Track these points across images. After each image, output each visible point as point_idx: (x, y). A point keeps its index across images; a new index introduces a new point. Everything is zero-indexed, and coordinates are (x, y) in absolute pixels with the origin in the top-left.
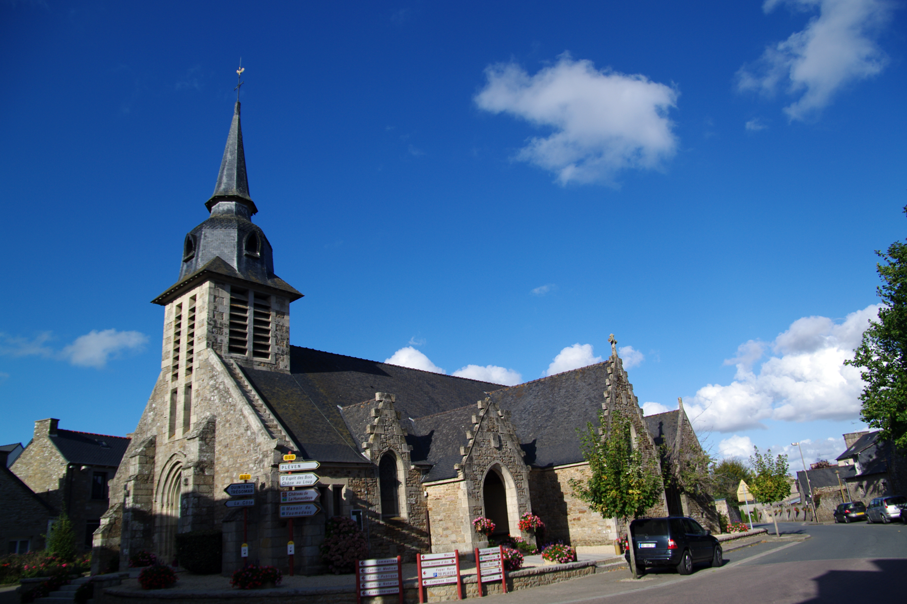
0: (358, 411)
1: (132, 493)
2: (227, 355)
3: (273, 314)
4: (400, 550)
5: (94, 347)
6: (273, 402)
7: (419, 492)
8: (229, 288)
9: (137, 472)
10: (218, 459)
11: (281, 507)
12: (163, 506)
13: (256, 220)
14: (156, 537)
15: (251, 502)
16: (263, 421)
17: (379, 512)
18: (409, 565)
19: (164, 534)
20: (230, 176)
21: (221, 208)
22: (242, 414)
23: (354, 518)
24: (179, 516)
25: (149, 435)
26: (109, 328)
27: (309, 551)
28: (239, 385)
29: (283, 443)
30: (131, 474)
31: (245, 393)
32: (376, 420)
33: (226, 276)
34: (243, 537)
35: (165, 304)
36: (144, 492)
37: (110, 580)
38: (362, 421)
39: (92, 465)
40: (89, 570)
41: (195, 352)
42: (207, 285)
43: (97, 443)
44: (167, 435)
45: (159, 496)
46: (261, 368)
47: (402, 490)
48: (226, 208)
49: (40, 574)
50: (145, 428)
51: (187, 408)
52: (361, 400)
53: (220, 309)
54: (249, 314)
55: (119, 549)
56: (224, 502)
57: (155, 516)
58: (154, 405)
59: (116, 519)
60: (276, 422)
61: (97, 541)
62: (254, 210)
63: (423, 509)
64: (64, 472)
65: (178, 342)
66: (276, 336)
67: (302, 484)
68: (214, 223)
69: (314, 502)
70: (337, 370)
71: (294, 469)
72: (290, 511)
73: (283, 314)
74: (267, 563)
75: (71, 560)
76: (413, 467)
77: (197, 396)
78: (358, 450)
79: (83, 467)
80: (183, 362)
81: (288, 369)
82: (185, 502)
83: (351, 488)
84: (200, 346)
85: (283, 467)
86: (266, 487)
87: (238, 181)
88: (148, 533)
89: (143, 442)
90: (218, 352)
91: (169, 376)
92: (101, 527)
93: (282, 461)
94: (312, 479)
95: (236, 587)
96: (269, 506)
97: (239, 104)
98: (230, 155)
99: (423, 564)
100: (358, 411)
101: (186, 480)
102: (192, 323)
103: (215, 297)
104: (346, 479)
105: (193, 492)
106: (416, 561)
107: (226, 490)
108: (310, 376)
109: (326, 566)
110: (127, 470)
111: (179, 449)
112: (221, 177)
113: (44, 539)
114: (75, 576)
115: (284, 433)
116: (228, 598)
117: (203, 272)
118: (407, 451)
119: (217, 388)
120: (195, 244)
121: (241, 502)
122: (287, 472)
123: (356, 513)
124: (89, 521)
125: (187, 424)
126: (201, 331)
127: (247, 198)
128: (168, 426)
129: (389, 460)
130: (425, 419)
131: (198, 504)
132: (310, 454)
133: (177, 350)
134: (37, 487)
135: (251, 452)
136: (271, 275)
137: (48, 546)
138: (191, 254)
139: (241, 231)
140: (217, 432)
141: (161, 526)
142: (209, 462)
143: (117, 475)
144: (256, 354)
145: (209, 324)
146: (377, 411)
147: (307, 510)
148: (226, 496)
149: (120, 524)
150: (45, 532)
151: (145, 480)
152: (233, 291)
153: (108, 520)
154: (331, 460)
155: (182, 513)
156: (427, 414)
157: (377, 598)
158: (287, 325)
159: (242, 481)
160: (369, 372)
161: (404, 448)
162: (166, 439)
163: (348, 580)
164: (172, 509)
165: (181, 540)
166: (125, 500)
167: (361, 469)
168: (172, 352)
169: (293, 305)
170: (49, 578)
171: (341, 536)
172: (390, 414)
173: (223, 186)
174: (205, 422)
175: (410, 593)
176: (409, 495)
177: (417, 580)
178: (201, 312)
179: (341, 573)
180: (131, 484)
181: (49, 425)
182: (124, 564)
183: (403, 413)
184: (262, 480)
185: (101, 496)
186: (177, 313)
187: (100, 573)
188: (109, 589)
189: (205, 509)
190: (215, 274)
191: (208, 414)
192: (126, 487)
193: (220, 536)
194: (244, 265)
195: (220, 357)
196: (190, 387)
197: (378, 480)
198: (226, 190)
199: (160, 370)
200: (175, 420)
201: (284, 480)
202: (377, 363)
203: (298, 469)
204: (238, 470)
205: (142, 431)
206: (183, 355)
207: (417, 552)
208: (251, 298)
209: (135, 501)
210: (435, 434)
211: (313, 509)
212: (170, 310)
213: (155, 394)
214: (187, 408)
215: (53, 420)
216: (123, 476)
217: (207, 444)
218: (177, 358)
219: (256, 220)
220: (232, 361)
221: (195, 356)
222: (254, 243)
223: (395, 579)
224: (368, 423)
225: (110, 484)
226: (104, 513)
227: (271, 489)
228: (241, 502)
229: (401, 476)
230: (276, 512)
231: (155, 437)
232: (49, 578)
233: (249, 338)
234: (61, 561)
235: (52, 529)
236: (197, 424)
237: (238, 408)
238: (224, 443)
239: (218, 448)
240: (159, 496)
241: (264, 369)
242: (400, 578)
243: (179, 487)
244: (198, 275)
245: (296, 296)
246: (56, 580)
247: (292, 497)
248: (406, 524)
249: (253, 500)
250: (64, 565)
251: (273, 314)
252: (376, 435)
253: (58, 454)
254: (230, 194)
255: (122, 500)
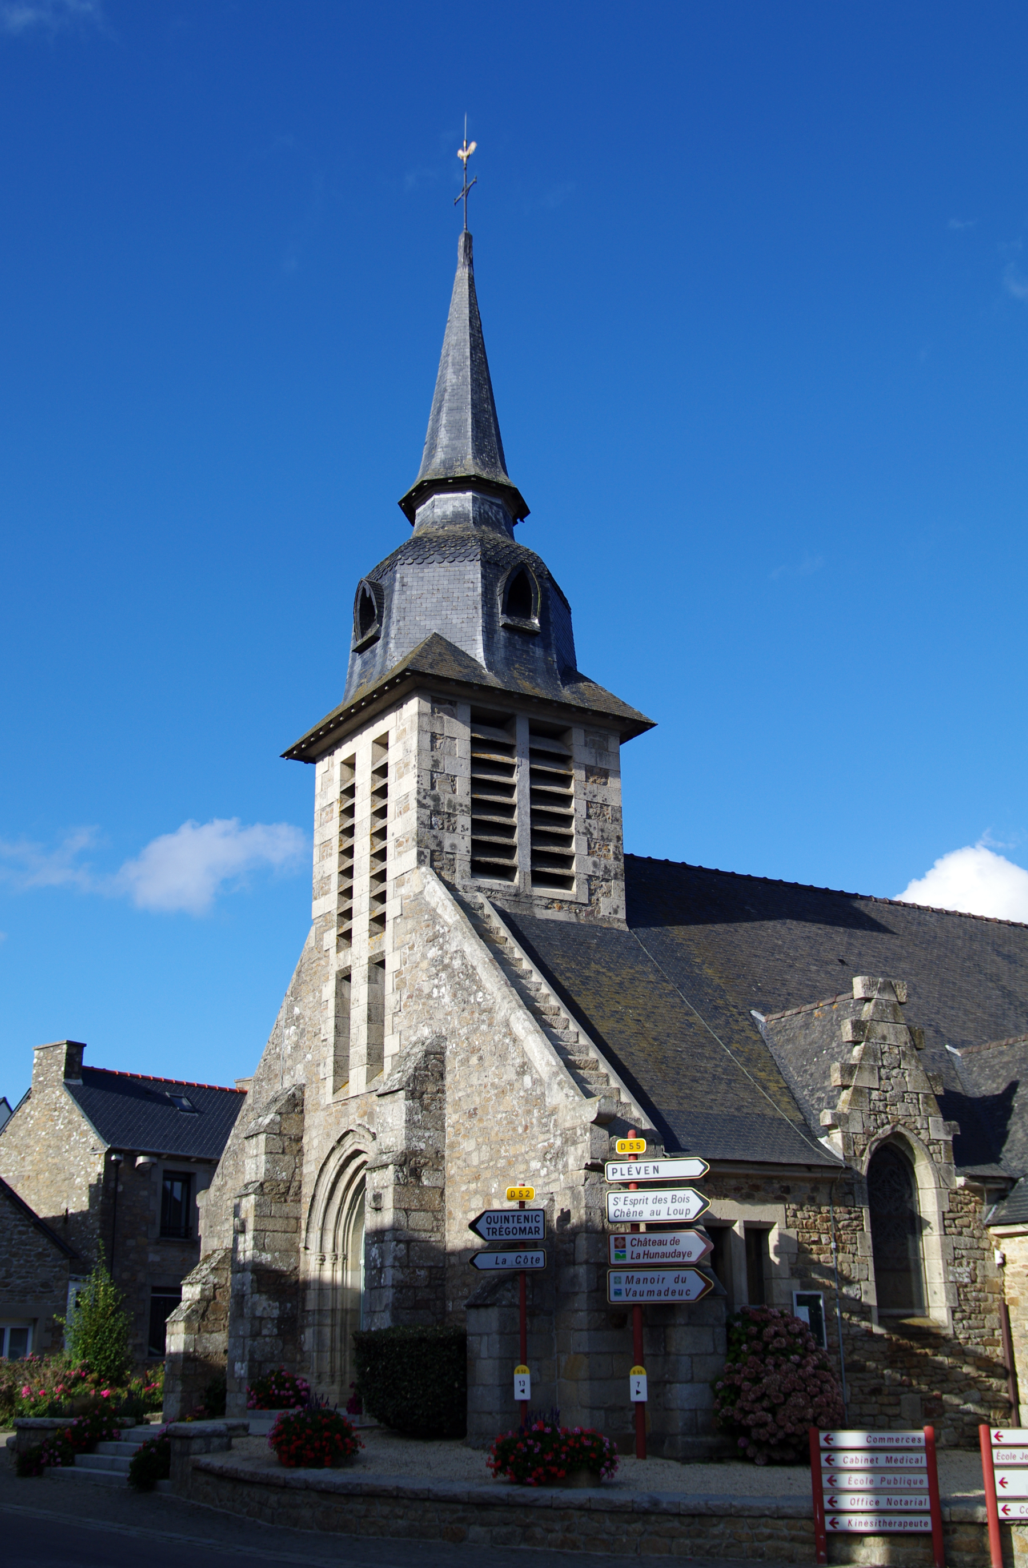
0: (807, 1026)
1: (250, 1225)
2: (468, 882)
3: (578, 775)
4: (931, 1411)
5: (187, 864)
6: (584, 1002)
7: (980, 1252)
8: (466, 712)
9: (261, 1176)
10: (452, 1146)
11: (613, 1275)
12: (323, 1260)
13: (526, 536)
14: (308, 1337)
15: (536, 1259)
16: (561, 1051)
17: (871, 1299)
18: (957, 1454)
19: (327, 1331)
20: (455, 428)
21: (438, 511)
22: (509, 1033)
23: (803, 1314)
24: (361, 1285)
25: (287, 1084)
26: (225, 816)
27: (686, 1396)
28: (500, 959)
29: (613, 1109)
30: (249, 1177)
31: (515, 980)
32: (857, 1050)
33: (458, 682)
34: (519, 1351)
35: (313, 760)
36: (280, 1224)
37: (206, 1436)
38: (818, 1053)
39: (158, 1155)
40: (158, 1407)
41: (390, 876)
42: (413, 706)
43: (170, 1102)
44: (330, 1083)
45: (314, 1236)
46: (554, 914)
47: (932, 1245)
48: (449, 510)
49: (54, 1410)
50: (277, 1067)
51: (375, 1016)
52: (814, 996)
53: (448, 765)
54: (520, 778)
55: (224, 1361)
56: (470, 1255)
57: (306, 1284)
58: (297, 1011)
59: (215, 1287)
60: (594, 1054)
61: (176, 1341)
62: (521, 511)
63: (992, 1301)
64: (100, 1168)
65: (349, 852)
66: (588, 832)
67: (663, 1217)
68: (422, 549)
69: (697, 1266)
70: (749, 918)
71: (642, 1176)
72: (634, 1287)
73: (605, 774)
74: (577, 1420)
75: (119, 1381)
76: (960, 1181)
77: (398, 988)
78: (810, 1132)
79: (141, 1160)
80: (361, 903)
81: (622, 915)
82: (375, 1251)
83: (792, 1233)
84: (402, 861)
85: (615, 1172)
86: (574, 1220)
87: (475, 438)
88: (290, 1326)
89: (275, 1100)
90: (445, 874)
91: (331, 937)
92: (183, 1305)
93: (611, 1155)
94: (688, 1204)
95: (501, 1477)
96: (582, 1270)
97: (469, 238)
98: (454, 374)
99: (999, 1456)
100: (807, 1026)
101: (377, 1197)
102: (380, 804)
103: (434, 737)
104: (780, 1208)
105: (395, 1229)
106: (976, 1446)
107: (473, 1226)
108: (678, 933)
109: (731, 1440)
110: (239, 1168)
111: (360, 1118)
112: (435, 432)
113: (61, 1326)
114: (128, 1420)
115: (615, 1082)
116: (484, 1504)
117: (401, 675)
118: (943, 1136)
119: (446, 967)
120: (381, 606)
121: (511, 1259)
122: (626, 1185)
123: (810, 1302)
124: (155, 1289)
125: (375, 1056)
126: (403, 823)
127: (502, 479)
128: (330, 1061)
129: (892, 1162)
130: (990, 1050)
131: (406, 1258)
132: (683, 1140)
133: (348, 873)
134: (44, 1205)
135: (531, 1132)
136: (570, 674)
137: (68, 1344)
138: (370, 633)
139: (490, 565)
140: (449, 1079)
141: (320, 1311)
142: (430, 1153)
143: (217, 1181)
144: (539, 879)
145: (421, 805)
146: (858, 1026)
147: (680, 1286)
148: (475, 1240)
149: (225, 1301)
150: (63, 1311)
151: (279, 1192)
152: (476, 721)
153: (198, 1288)
154: (737, 1156)
155: (368, 1280)
156: (997, 1036)
157: (870, 1540)
158: (615, 801)
159: (514, 1205)
160: (832, 920)
161: (937, 1129)
162: (327, 1096)
163: (787, 1484)
164: (344, 1269)
165: (368, 1348)
166: (235, 1241)
167: (819, 1183)
168: (335, 878)
169: (630, 751)
170: (74, 1421)
171: (770, 1360)
172: (893, 1035)
173: (440, 456)
174: (418, 1051)
175: (964, 1537)
176: (953, 1259)
177: (981, 1501)
178: (401, 776)
179: (771, 1462)
180: (249, 1203)
181: (63, 1058)
182: (237, 1399)
183: (930, 1033)
184: (563, 1203)
185: (180, 1229)
186: (343, 781)
187: (182, 1419)
188: (205, 1459)
189: (422, 1273)
190: (430, 680)
191: (426, 1032)
192: (236, 1211)
193: (459, 1343)
194: (501, 654)
195: (450, 887)
196: (382, 964)
197: (866, 1213)
198: (448, 464)
199: (310, 922)
200: (347, 1047)
201: (622, 1206)
202: (856, 896)
203: (652, 1175)
204: (503, 1174)
205: (270, 1075)
206: (362, 883)
207: (979, 1420)
208: (522, 736)
209: (259, 1245)
210: (1021, 1091)
211: (694, 1286)
212: (328, 772)
213: (300, 983)
214: (375, 1016)
215: (70, 1044)
216: (230, 1183)
217: (425, 1108)
218: (347, 893)
219: (526, 536)
220: (481, 898)
221: (389, 886)
222: (524, 595)
223: (919, 1491)
224: (833, 1058)
225: (202, 1200)
226: (188, 1271)
227: (586, 1228)
228: (511, 1259)
229: (929, 1203)
230: (600, 1287)
231: (301, 1088)
232: (74, 1421)
233: (521, 838)
234: (98, 1383)
235: (77, 1305)
236: (402, 1058)
237: (500, 1016)
238: (467, 1106)
239: (451, 1118)
240: (314, 1236)
241: (561, 916)
242: (933, 1489)
243: (361, 1213)
244: (391, 683)
245: (634, 727)
246: (86, 1428)
247: (640, 1250)
248: (945, 1339)
249: (540, 1255)
250: (105, 1393)
251: (578, 775)
252: (858, 1091)
253: (86, 1125)
254: (460, 472)
255: (228, 1243)
